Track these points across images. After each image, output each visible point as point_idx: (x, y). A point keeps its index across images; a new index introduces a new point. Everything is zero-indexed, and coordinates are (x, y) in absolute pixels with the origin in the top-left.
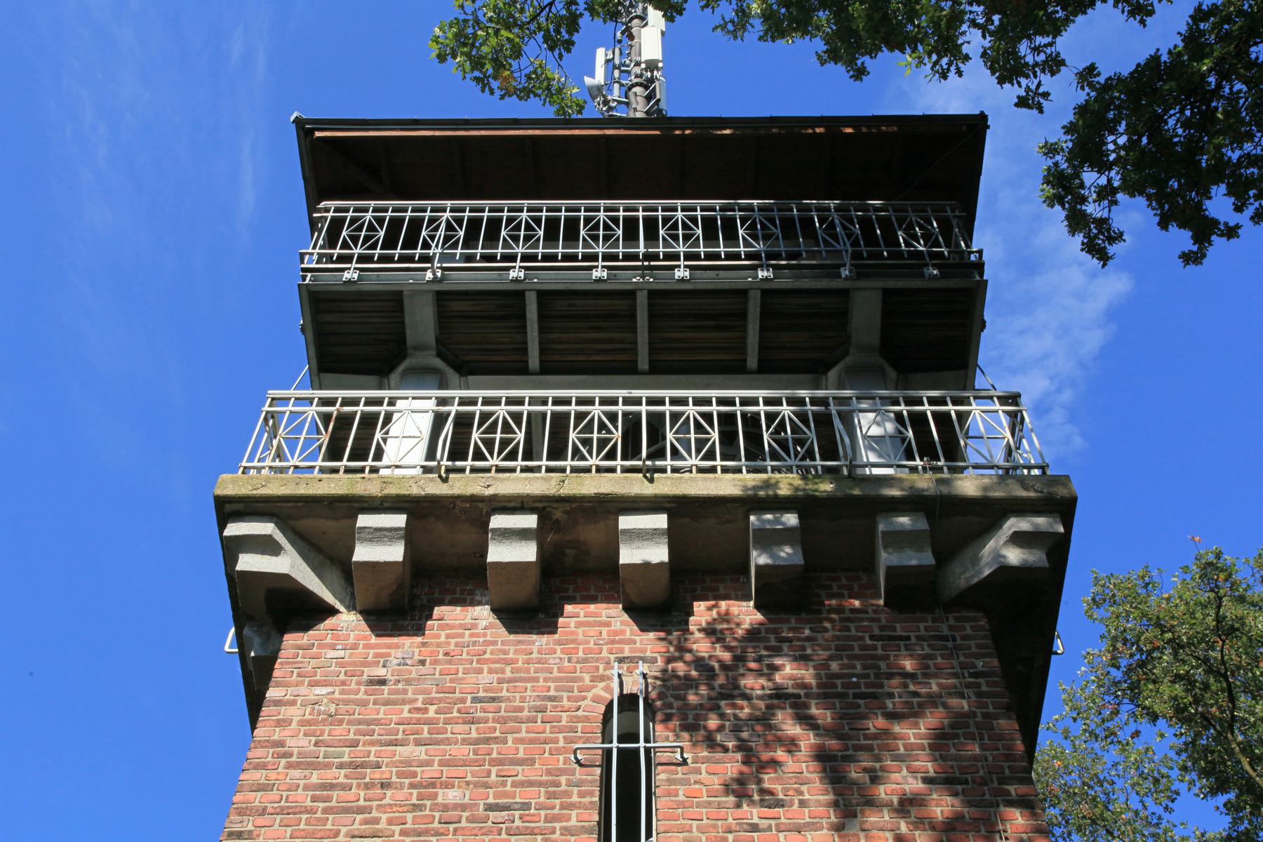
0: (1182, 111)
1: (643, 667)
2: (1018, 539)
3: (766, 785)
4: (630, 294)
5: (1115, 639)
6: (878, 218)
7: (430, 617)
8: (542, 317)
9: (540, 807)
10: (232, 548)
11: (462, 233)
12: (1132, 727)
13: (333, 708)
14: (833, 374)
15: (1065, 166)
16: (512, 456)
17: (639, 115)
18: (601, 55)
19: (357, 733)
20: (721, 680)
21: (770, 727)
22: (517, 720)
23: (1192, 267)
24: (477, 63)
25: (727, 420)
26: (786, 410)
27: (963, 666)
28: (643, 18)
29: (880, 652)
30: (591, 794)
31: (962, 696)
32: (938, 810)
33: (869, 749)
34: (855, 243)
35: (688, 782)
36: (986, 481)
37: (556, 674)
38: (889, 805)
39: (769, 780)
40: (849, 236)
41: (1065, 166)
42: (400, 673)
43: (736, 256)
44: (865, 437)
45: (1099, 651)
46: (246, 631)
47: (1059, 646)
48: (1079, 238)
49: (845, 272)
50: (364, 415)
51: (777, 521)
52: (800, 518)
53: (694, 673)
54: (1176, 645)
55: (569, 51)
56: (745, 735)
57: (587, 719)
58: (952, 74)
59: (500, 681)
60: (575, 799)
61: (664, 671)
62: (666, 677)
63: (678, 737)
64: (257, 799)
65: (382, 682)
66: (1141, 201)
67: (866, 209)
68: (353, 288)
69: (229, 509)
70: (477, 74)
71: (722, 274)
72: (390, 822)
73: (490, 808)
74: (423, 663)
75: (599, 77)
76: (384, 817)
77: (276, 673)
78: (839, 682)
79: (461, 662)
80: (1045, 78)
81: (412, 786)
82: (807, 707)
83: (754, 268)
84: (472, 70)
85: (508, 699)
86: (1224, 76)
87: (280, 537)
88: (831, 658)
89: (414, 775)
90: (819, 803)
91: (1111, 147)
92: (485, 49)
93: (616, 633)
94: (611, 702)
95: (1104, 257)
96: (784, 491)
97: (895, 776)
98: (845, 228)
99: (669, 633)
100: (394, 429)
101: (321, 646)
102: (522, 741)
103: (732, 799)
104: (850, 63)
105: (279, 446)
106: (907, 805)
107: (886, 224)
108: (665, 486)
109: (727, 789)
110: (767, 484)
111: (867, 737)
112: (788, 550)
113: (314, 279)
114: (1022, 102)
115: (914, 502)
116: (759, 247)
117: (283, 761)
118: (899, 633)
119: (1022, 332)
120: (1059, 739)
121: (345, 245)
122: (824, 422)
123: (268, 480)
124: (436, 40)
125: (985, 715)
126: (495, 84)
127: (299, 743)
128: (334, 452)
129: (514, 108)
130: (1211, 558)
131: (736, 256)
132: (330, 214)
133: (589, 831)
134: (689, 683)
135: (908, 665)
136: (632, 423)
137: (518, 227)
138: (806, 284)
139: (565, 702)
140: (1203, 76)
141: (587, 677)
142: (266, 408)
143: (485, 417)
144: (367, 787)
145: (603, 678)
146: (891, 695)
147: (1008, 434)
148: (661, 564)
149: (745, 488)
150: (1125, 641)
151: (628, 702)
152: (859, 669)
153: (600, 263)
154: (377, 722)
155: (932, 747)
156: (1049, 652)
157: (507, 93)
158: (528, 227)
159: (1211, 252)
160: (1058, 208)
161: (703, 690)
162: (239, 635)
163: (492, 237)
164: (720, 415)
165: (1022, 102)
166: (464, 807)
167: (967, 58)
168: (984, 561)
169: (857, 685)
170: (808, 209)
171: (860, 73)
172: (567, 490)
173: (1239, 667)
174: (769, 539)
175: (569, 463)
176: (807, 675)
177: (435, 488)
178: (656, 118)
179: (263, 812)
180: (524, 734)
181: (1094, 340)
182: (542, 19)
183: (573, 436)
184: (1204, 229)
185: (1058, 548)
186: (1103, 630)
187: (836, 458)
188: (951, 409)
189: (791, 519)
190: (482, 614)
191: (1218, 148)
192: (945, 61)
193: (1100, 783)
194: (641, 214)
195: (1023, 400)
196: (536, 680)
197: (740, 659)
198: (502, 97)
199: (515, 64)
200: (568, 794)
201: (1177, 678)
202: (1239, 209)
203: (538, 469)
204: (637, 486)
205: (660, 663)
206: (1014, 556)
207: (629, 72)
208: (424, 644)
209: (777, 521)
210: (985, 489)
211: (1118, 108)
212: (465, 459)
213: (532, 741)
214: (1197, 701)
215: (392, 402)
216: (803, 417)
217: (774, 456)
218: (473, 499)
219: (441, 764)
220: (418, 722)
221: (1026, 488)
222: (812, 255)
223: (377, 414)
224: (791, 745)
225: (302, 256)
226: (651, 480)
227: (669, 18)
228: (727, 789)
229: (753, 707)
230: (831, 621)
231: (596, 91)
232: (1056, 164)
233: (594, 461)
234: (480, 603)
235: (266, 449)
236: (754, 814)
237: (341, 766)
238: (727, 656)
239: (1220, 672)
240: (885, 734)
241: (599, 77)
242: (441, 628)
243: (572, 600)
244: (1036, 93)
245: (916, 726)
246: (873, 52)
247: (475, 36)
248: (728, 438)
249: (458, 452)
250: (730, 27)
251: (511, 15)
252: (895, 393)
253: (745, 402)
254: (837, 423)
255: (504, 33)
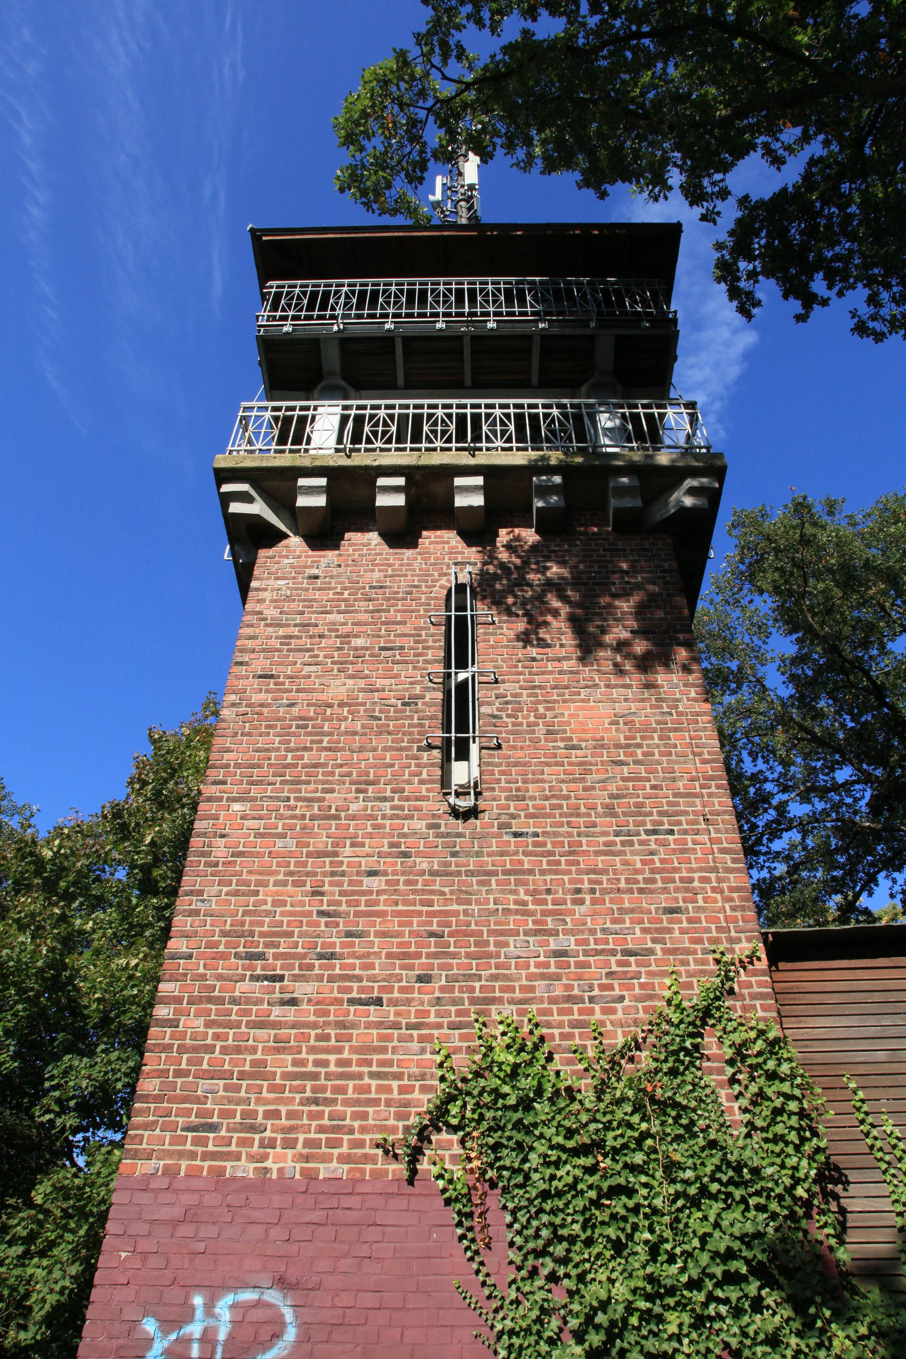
0: (799, 225)
1: (469, 568)
2: (691, 491)
3: (541, 636)
4: (459, 338)
5: (743, 547)
6: (614, 289)
7: (343, 539)
8: (405, 353)
9: (411, 648)
10: (226, 499)
11: (355, 301)
12: (749, 598)
13: (289, 593)
14: (584, 388)
15: (728, 257)
16: (389, 441)
17: (464, 221)
18: (439, 181)
19: (304, 606)
20: (515, 576)
21: (544, 603)
22: (395, 599)
23: (801, 324)
24: (364, 193)
25: (519, 418)
26: (555, 412)
27: (657, 566)
28: (465, 156)
29: (608, 558)
30: (440, 641)
31: (655, 584)
32: (639, 648)
33: (601, 614)
34: (599, 306)
35: (495, 634)
36: (674, 456)
37: (418, 572)
38: (611, 646)
39: (542, 633)
40: (595, 301)
41: (728, 257)
42: (326, 572)
43: (525, 314)
44: (603, 428)
45: (733, 553)
46: (236, 548)
47: (712, 554)
48: (735, 303)
49: (593, 324)
50: (299, 417)
51: (549, 480)
52: (563, 479)
53: (499, 571)
54: (777, 550)
55: (421, 184)
56: (529, 607)
57: (436, 598)
58: (661, 199)
59: (385, 576)
60: (430, 644)
61: (482, 570)
62: (483, 573)
63: (490, 609)
64: (250, 644)
65: (317, 577)
66: (772, 281)
67: (606, 283)
68: (289, 337)
69: (224, 475)
70: (364, 200)
71: (517, 325)
72: (325, 657)
73: (382, 649)
74: (339, 566)
75: (438, 196)
76: (322, 654)
77: (255, 572)
78: (584, 576)
79: (362, 565)
80: (719, 202)
81: (337, 637)
82: (565, 590)
83: (536, 321)
84: (361, 197)
85: (390, 587)
86: (825, 203)
87: (253, 492)
88: (579, 562)
89: (337, 630)
90: (571, 646)
91: (756, 246)
92: (369, 183)
93: (453, 548)
94: (450, 591)
95: (748, 315)
96: (553, 462)
97: (615, 630)
98: (592, 295)
99: (484, 548)
100: (317, 425)
101: (280, 557)
102: (399, 611)
103: (521, 644)
104: (597, 188)
105: (250, 437)
106: (621, 646)
107: (617, 293)
108: (482, 459)
109: (518, 639)
110: (543, 458)
111: (599, 608)
112: (555, 498)
113: (266, 331)
114: (704, 218)
115: (631, 469)
116: (539, 308)
117: (263, 623)
118: (620, 547)
119: (692, 366)
120: (707, 605)
121: (283, 310)
122: (578, 418)
123: (244, 458)
124: (338, 178)
125: (668, 595)
126: (375, 206)
127: (271, 612)
128: (282, 440)
129: (387, 220)
130: (800, 500)
131: (525, 314)
132: (274, 290)
133: (439, 662)
134: (496, 577)
135: (625, 566)
136: (462, 419)
137: (389, 296)
138: (568, 331)
139: (424, 589)
140: (813, 202)
141: (436, 574)
142: (241, 414)
143: (372, 417)
144: (311, 637)
145: (445, 574)
146: (614, 584)
147: (688, 427)
148: (479, 507)
149: (530, 461)
150: (749, 548)
151: (460, 588)
152: (596, 568)
153: (441, 319)
154: (315, 600)
155: (637, 613)
156: (706, 557)
157: (383, 212)
158: (396, 296)
159: (812, 314)
160: (723, 284)
161: (505, 582)
162: (232, 549)
163: (374, 303)
164: (515, 414)
165: (704, 218)
166: (366, 649)
167: (670, 188)
168: (671, 505)
169: (595, 578)
170: (570, 283)
171: (603, 195)
172: (422, 462)
173: (811, 563)
174: (544, 491)
175: (424, 445)
176: (565, 572)
177: (343, 461)
178: (474, 223)
179: (253, 651)
180: (400, 607)
181: (734, 372)
182: (404, 164)
183: (426, 428)
184: (809, 300)
185: (713, 497)
186: (737, 542)
187: (585, 442)
188: (655, 411)
189: (557, 479)
190: (374, 537)
191: (820, 249)
192: (657, 189)
193: (729, 629)
194: (466, 286)
195: (698, 406)
196: (406, 575)
197: (526, 563)
198: (380, 215)
199: (387, 192)
200: (426, 641)
201: (777, 569)
202: (830, 288)
203: (404, 449)
204: (465, 459)
205: (479, 565)
206: (688, 501)
207: (457, 192)
208: (340, 555)
209: (549, 480)
210: (673, 461)
211: (762, 221)
212: (361, 443)
213: (405, 611)
214: (786, 582)
215: (315, 409)
216: (565, 416)
217: (548, 440)
218: (367, 468)
219: (353, 624)
220: (339, 600)
221: (697, 461)
222: (572, 313)
223: (307, 416)
224: (556, 613)
225: (258, 317)
226: (474, 456)
227: (484, 161)
228: (518, 639)
229: (533, 590)
230: (580, 540)
231: (436, 205)
232: (723, 256)
233: (438, 444)
234: (372, 531)
235: (242, 437)
236: (533, 652)
237: (295, 625)
238: (518, 561)
239: (799, 565)
240: (610, 606)
241: (438, 196)
242: (350, 545)
243: (427, 529)
244: (713, 212)
245: (628, 601)
246: (613, 182)
247: (362, 174)
248: (520, 428)
249: (357, 439)
250: (522, 165)
251: (385, 161)
252: (621, 401)
253: (531, 406)
254: (587, 421)
255: (381, 173)
